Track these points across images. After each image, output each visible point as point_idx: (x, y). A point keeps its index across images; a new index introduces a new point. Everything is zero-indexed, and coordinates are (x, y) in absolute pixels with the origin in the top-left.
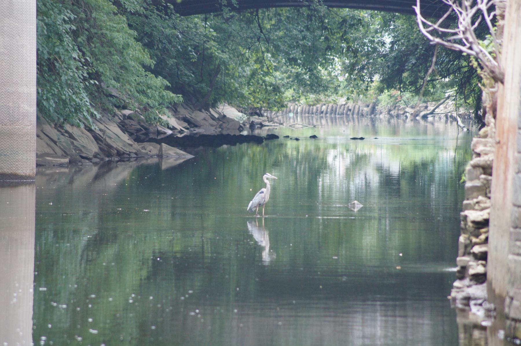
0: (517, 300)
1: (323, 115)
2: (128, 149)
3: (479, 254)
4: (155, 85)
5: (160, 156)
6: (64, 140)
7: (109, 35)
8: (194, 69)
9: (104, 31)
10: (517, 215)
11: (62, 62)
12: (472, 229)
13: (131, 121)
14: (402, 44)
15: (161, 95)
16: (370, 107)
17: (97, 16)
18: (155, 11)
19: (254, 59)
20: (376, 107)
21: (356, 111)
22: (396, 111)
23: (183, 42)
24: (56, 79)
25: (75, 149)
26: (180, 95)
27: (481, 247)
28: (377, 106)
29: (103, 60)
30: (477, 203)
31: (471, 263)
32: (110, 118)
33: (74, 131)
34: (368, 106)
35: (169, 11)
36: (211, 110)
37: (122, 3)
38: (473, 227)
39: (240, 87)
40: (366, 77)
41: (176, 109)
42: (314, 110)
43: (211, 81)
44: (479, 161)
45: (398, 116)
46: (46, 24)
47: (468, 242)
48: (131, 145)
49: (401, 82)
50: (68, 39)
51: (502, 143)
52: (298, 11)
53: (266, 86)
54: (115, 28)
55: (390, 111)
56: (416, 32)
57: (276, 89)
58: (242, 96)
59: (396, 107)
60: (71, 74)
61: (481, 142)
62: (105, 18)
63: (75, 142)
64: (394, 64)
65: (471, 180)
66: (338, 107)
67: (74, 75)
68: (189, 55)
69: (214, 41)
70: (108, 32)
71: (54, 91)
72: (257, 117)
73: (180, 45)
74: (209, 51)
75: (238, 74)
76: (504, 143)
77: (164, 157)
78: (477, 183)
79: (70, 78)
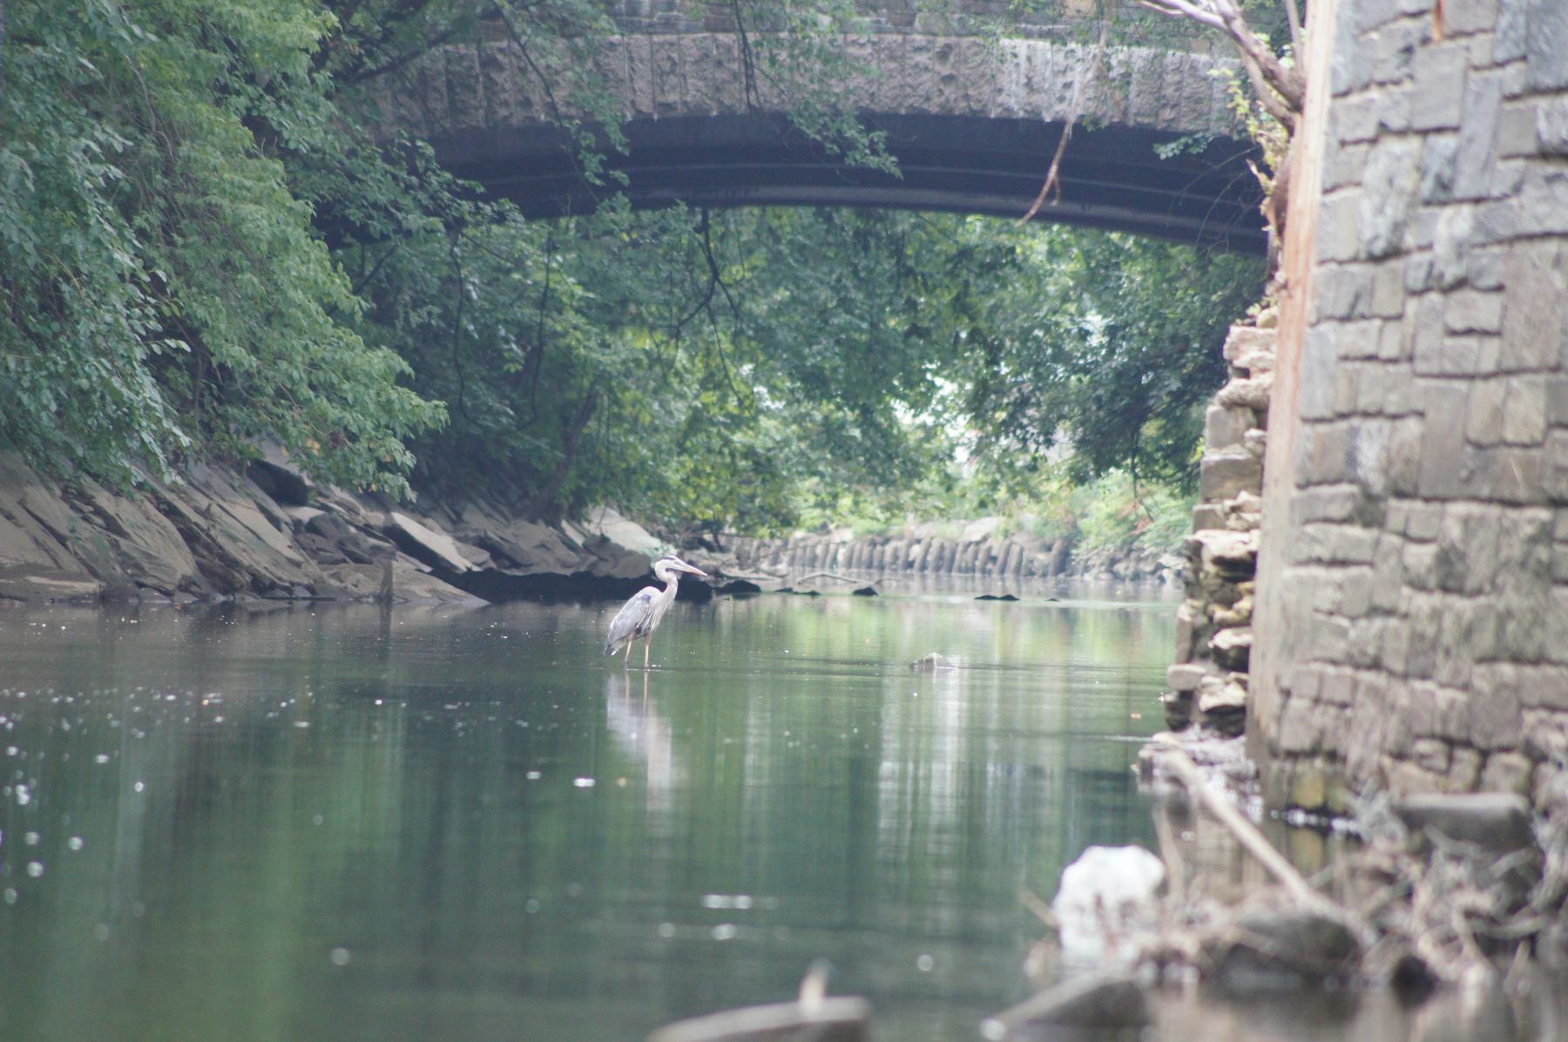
0: (1301, 697)
1: (915, 571)
2: (286, 575)
3: (1232, 654)
4: (367, 368)
5: (385, 600)
6: (89, 534)
7: (228, 211)
8: (514, 396)
9: (215, 199)
10: (1310, 446)
11: (83, 284)
12: (1214, 583)
13: (317, 538)
14: (1143, 334)
15: (383, 399)
16: (1055, 551)
17: (193, 154)
18: (379, 162)
19: (700, 375)
20: (1074, 551)
21: (1013, 563)
22: (1132, 565)
23: (483, 311)
24: (63, 332)
25: (123, 564)
26: (442, 403)
27: (1238, 635)
28: (1076, 547)
29: (209, 285)
30: (1234, 509)
31: (1207, 680)
32: (236, 484)
33: (124, 511)
34: (1049, 549)
35: (420, 164)
36: (564, 524)
37: (274, 124)
38: (1217, 575)
39: (654, 459)
40: (1030, 429)
41: (459, 516)
42: (888, 558)
43: (567, 438)
44: (1244, 387)
45: (1137, 577)
46: (35, 166)
47: (1203, 620)
48: (298, 565)
49: (1135, 451)
50: (100, 212)
51: (1291, 284)
52: (829, 219)
53: (732, 455)
54: (249, 190)
55: (1113, 561)
56: (1181, 300)
57: (763, 466)
58: (662, 485)
59: (1130, 551)
60: (108, 318)
61: (1255, 337)
62: (217, 158)
63: (123, 542)
64: (1115, 394)
65: (1219, 444)
66: (960, 548)
67: (117, 320)
68: (500, 353)
69: (578, 311)
70: (225, 202)
71: (56, 363)
72: (703, 551)
73: (474, 320)
74: (562, 342)
75: (648, 419)
76: (1297, 282)
77: (396, 600)
78: (1236, 453)
79: (102, 327)
